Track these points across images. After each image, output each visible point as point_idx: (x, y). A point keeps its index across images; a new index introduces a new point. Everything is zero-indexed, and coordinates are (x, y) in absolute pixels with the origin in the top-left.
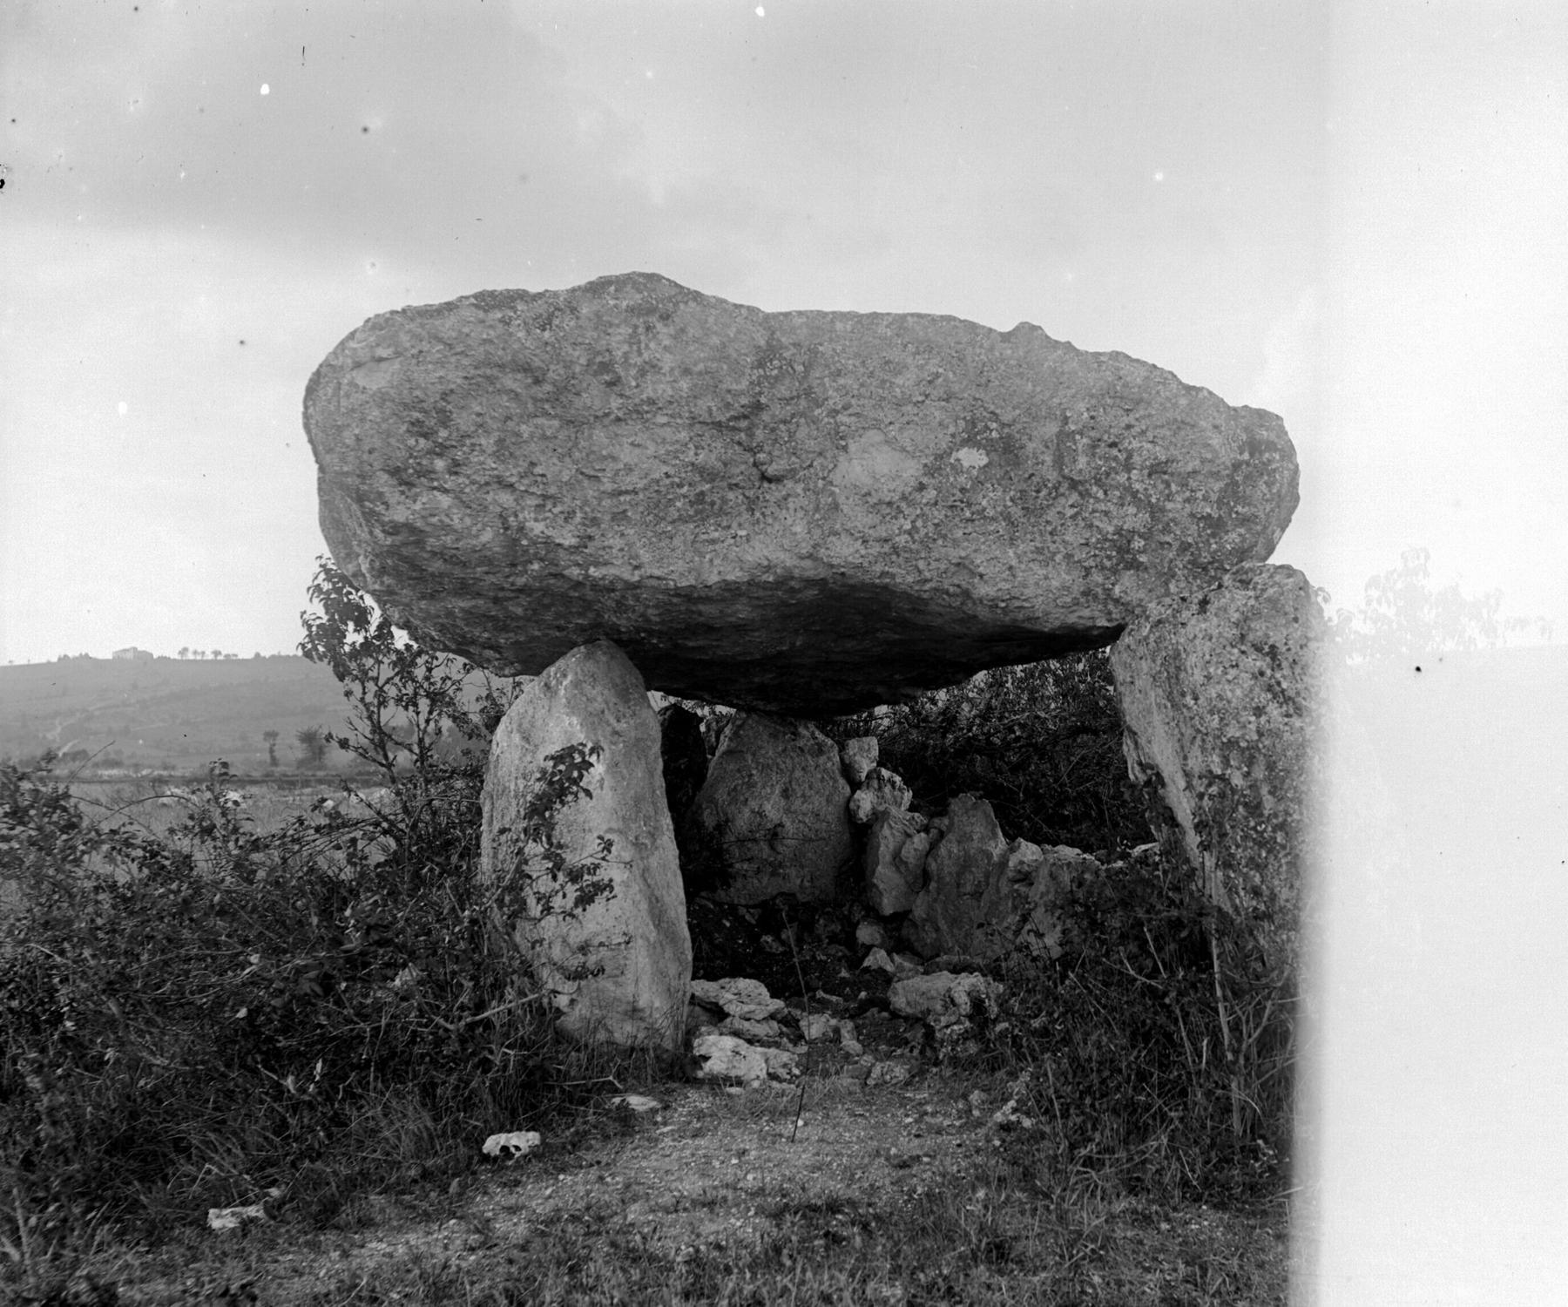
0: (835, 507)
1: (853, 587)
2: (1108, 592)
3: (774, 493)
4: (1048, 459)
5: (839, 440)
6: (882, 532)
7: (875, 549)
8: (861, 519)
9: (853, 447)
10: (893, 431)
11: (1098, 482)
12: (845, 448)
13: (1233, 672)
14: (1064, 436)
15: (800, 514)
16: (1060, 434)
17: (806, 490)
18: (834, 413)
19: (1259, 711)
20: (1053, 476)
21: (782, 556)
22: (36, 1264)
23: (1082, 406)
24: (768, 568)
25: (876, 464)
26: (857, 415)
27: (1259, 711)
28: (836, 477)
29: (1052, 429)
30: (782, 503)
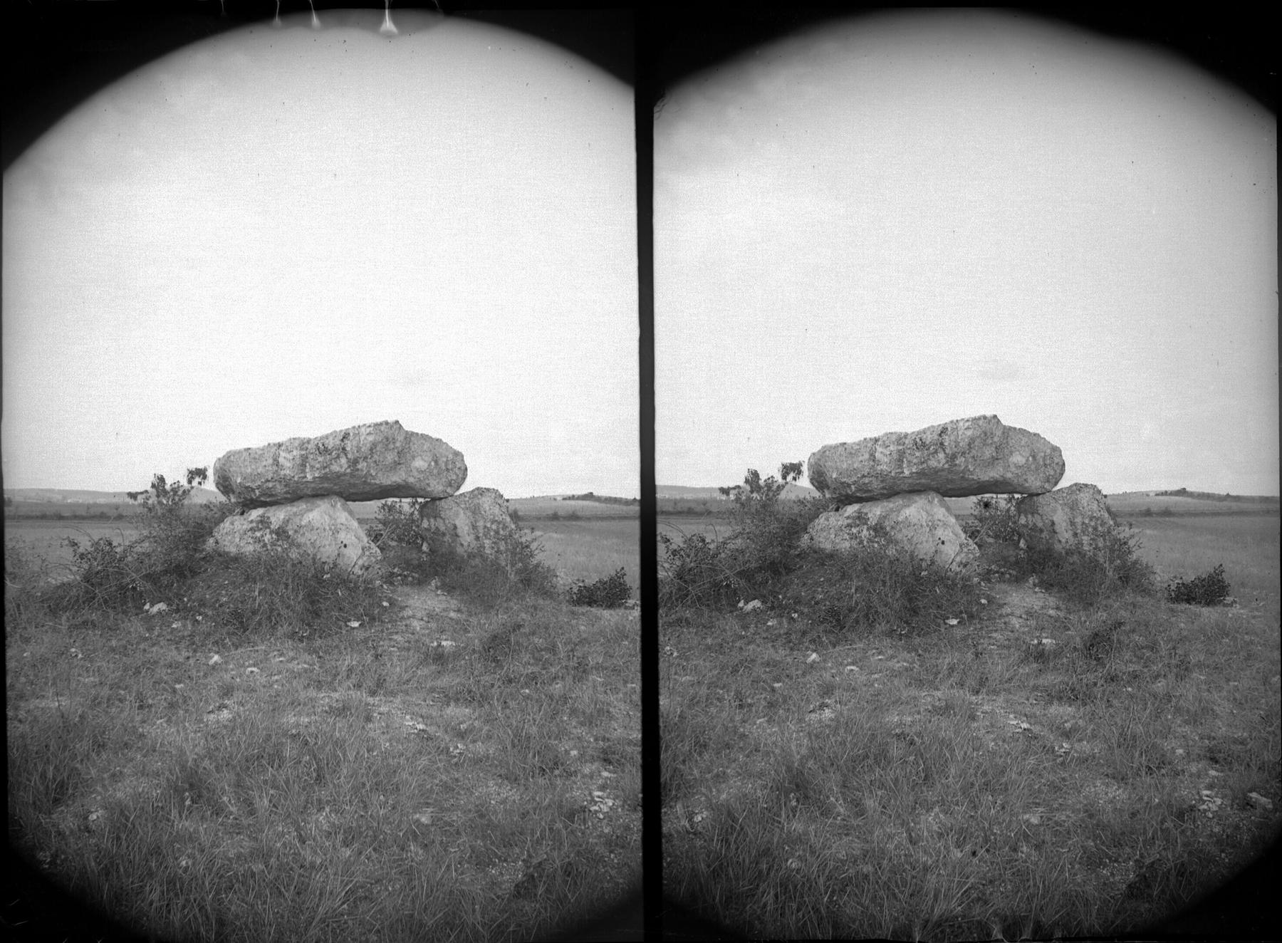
8: (416, 474)
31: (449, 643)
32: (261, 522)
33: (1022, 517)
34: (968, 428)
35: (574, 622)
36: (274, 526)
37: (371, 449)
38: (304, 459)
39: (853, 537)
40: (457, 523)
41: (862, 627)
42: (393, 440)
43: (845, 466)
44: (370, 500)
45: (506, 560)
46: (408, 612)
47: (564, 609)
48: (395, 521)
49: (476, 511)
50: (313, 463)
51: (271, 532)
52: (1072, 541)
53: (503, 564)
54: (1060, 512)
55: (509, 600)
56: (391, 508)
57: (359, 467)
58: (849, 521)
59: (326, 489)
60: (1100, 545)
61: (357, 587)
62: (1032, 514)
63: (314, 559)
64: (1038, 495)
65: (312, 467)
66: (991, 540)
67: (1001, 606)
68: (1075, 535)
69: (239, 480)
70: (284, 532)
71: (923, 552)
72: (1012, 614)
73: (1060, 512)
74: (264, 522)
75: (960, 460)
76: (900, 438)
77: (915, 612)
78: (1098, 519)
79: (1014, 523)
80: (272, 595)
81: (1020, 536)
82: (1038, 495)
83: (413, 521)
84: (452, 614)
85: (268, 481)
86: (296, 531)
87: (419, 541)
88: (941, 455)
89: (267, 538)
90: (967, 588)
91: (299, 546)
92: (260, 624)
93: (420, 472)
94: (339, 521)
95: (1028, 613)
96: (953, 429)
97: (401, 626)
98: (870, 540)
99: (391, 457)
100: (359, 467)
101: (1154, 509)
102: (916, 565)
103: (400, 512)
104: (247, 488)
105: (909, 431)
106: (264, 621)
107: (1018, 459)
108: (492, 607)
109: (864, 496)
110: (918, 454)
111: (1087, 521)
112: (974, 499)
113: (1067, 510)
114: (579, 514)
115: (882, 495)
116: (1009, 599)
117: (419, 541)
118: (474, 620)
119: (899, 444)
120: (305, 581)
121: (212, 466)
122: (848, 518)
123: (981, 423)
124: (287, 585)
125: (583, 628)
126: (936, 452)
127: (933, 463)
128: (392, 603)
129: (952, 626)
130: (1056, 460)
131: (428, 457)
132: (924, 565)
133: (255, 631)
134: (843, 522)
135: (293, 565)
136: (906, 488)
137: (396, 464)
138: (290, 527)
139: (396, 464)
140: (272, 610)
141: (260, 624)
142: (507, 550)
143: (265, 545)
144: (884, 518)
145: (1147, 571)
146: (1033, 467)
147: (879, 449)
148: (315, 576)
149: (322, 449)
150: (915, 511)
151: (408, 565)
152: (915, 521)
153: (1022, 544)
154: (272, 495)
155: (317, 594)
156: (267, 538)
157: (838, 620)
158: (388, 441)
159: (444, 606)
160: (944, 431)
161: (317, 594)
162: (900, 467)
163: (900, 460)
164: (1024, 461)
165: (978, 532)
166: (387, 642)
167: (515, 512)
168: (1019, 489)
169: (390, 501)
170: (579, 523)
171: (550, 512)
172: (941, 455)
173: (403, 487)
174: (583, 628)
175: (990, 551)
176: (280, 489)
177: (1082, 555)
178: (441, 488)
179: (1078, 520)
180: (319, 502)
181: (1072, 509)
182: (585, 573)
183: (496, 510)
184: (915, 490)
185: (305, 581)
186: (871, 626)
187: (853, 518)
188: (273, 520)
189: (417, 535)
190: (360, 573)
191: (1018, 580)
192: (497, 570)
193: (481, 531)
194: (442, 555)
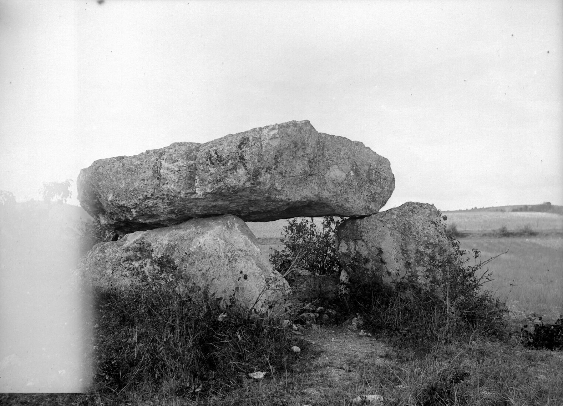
0: (326, 183)
1: (296, 203)
2: (368, 207)
3: (310, 178)
4: (365, 175)
5: (328, 167)
6: (335, 190)
7: (332, 194)
8: (330, 186)
9: (331, 169)
10: (340, 165)
11: (375, 181)
12: (329, 169)
13: (429, 228)
14: (370, 169)
15: (316, 184)
16: (369, 169)
17: (318, 178)
18: (327, 160)
19: (438, 236)
20: (366, 179)
21: (311, 194)
22: (471, 344)
23: (374, 163)
24: (305, 198)
25: (336, 173)
26: (333, 161)
27: (438, 236)
28: (326, 176)
29: (367, 168)
30: (311, 181)
31: (375, 397)
32: (141, 250)
33: (343, 244)
34: (274, 138)
35: (531, 370)
36: (157, 254)
37: (276, 158)
38: (193, 171)
39: (137, 272)
40: (383, 246)
41: (146, 386)
42: (302, 144)
43: (123, 185)
44: (273, 219)
45: (444, 292)
46: (324, 359)
47: (518, 353)
48: (306, 246)
49: (406, 231)
50: (203, 175)
51: (153, 262)
52: (404, 273)
53: (441, 296)
54: (388, 237)
55: (448, 342)
56: (301, 229)
57: (261, 179)
58: (131, 253)
59: (220, 208)
60: (439, 277)
61: (259, 329)
62: (355, 240)
63: (206, 293)
64: (362, 217)
65: (202, 180)
66: (305, 272)
67: (317, 354)
68: (408, 265)
69: (110, 198)
70: (169, 262)
71: (220, 289)
72: (331, 364)
73: (388, 237)
74: (143, 250)
75: (265, 177)
76: (191, 151)
77: (212, 364)
78: (435, 246)
79: (334, 251)
80: (154, 341)
81: (341, 267)
82: (362, 217)
83: (328, 244)
84: (379, 361)
85: (147, 198)
86: (183, 260)
87: (336, 269)
88: (241, 172)
89: (148, 268)
90: (276, 334)
91: (187, 279)
92: (140, 378)
93: (336, 184)
94: (236, 246)
95: (350, 363)
96: (255, 139)
97: (316, 376)
98: (155, 278)
99: (300, 167)
100: (261, 179)
101: (511, 228)
102: (215, 306)
103: (312, 233)
104: (120, 207)
105: (202, 141)
106: (145, 374)
107: (336, 173)
108: (429, 351)
109: (148, 222)
110: (212, 170)
111: (422, 249)
112: (283, 223)
113: (398, 235)
114: (534, 229)
115: (171, 220)
116: (327, 346)
117: (336, 269)
118: (405, 369)
119: (189, 159)
120: (197, 322)
121: (75, 179)
122: (127, 250)
123: (289, 131)
124: (173, 329)
125: (542, 377)
126: (235, 168)
127: (231, 181)
128: (304, 347)
129: (257, 381)
130: (383, 175)
131: (347, 168)
132: (222, 304)
133: (135, 387)
134: (120, 254)
135: (182, 304)
136: (199, 211)
137: (308, 175)
138: (176, 254)
139: (308, 175)
140: (155, 361)
141: (140, 378)
142: (445, 279)
143: (145, 278)
144: (171, 248)
145: (499, 309)
146: (355, 183)
147: (165, 164)
148: (208, 315)
149: (216, 159)
150: (209, 239)
151: (321, 298)
152: (210, 251)
153: (343, 276)
154: (152, 216)
155: (212, 340)
156: (148, 268)
157: (117, 377)
158: (297, 146)
159: (368, 350)
160: (244, 141)
161: (212, 340)
162: (192, 186)
163: (191, 179)
164: (344, 175)
165: (289, 262)
166: (299, 397)
167: (454, 228)
168: (339, 210)
169: (299, 220)
170: (534, 240)
171: (497, 227)
172: (241, 172)
173: (316, 203)
174: (542, 377)
175: (304, 287)
176: (162, 208)
177: (417, 290)
178: (362, 204)
179: (412, 247)
180: (211, 223)
181: (403, 234)
182: (544, 306)
183: (431, 230)
184: (210, 214)
185: (197, 322)
186: (157, 382)
187: (134, 249)
188: (154, 246)
189: (333, 260)
190: (264, 310)
191: (337, 322)
192: (433, 304)
193: (413, 256)
194: (365, 286)
